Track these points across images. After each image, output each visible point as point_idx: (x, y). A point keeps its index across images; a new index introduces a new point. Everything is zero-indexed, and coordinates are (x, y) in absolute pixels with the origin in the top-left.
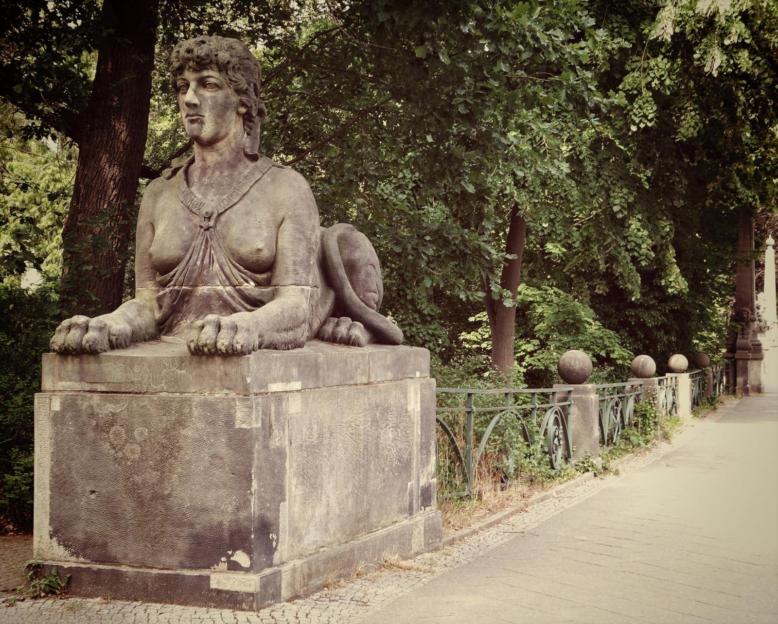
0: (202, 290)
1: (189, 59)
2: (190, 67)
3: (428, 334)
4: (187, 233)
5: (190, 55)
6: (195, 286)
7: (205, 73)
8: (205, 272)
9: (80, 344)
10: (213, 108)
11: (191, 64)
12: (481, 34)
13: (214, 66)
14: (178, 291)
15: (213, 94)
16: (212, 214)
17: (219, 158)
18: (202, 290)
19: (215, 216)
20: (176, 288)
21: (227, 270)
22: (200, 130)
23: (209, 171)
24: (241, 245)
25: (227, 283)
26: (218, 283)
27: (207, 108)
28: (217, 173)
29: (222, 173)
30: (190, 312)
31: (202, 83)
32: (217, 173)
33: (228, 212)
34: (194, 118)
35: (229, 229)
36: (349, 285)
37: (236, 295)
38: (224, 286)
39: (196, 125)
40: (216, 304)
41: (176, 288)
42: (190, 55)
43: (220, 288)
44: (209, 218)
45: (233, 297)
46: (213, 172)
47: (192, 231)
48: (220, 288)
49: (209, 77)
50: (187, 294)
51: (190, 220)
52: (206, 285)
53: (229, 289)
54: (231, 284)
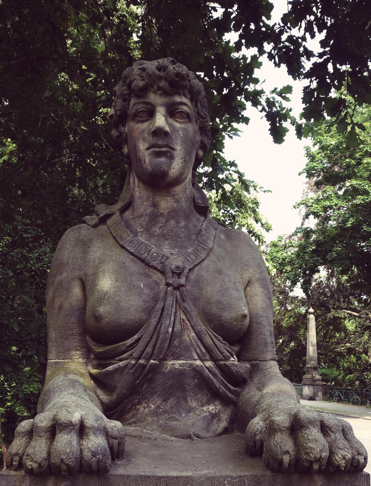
0: (175, 364)
1: (160, 78)
2: (159, 88)
3: (18, 378)
4: (147, 291)
5: (162, 74)
6: (165, 359)
7: (178, 99)
8: (176, 342)
9: (81, 459)
10: (184, 142)
11: (162, 84)
12: (134, 182)
13: (187, 92)
14: (144, 366)
15: (183, 126)
16: (184, 269)
17: (175, 205)
18: (175, 364)
19: (186, 271)
20: (142, 361)
21: (208, 340)
22: (170, 165)
23: (162, 220)
24: (224, 309)
25: (208, 357)
26: (197, 357)
27: (179, 141)
28: (172, 222)
29: (178, 222)
30: (153, 394)
31: (172, 112)
32: (172, 222)
33: (196, 269)
34: (164, 149)
35: (202, 289)
36: (123, 356)
37: (217, 372)
38: (202, 360)
39: (163, 159)
40: (191, 382)
41: (142, 361)
42: (162, 74)
43: (198, 363)
44: (179, 275)
45: (214, 375)
46: (167, 221)
47: (152, 289)
48: (198, 363)
49: (182, 103)
50: (155, 369)
51: (148, 276)
52: (178, 358)
53: (209, 364)
54: (213, 359)
